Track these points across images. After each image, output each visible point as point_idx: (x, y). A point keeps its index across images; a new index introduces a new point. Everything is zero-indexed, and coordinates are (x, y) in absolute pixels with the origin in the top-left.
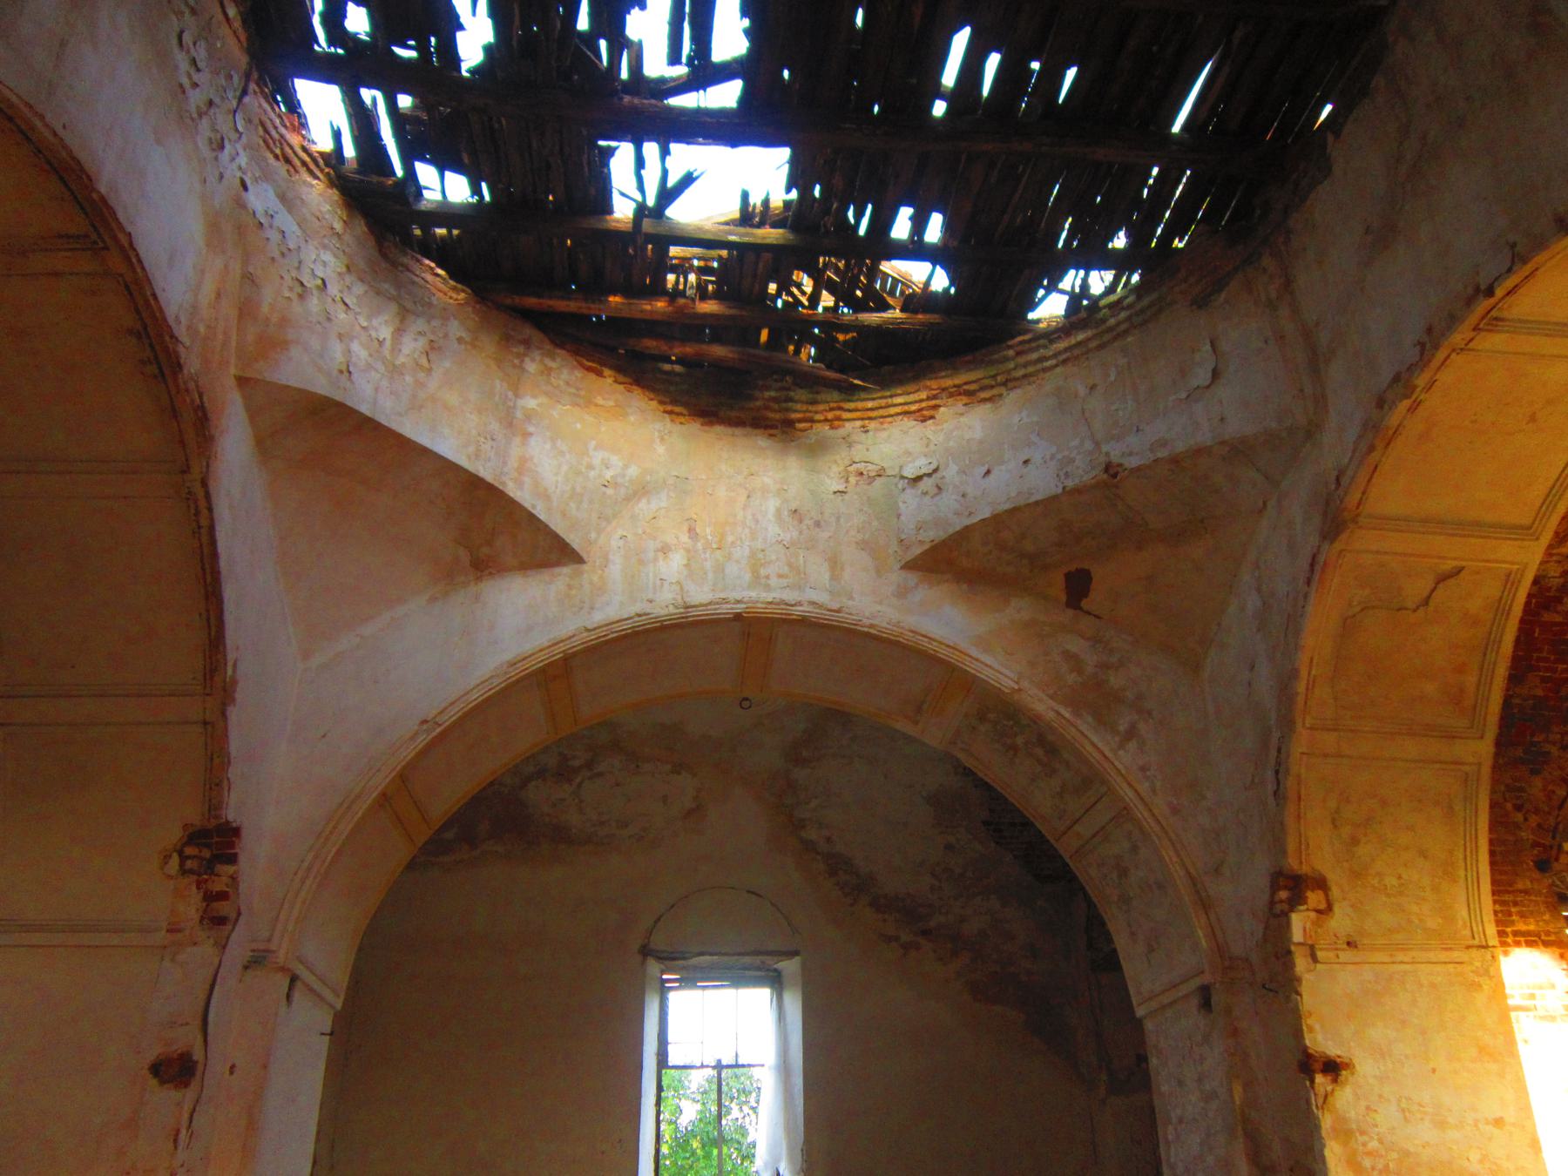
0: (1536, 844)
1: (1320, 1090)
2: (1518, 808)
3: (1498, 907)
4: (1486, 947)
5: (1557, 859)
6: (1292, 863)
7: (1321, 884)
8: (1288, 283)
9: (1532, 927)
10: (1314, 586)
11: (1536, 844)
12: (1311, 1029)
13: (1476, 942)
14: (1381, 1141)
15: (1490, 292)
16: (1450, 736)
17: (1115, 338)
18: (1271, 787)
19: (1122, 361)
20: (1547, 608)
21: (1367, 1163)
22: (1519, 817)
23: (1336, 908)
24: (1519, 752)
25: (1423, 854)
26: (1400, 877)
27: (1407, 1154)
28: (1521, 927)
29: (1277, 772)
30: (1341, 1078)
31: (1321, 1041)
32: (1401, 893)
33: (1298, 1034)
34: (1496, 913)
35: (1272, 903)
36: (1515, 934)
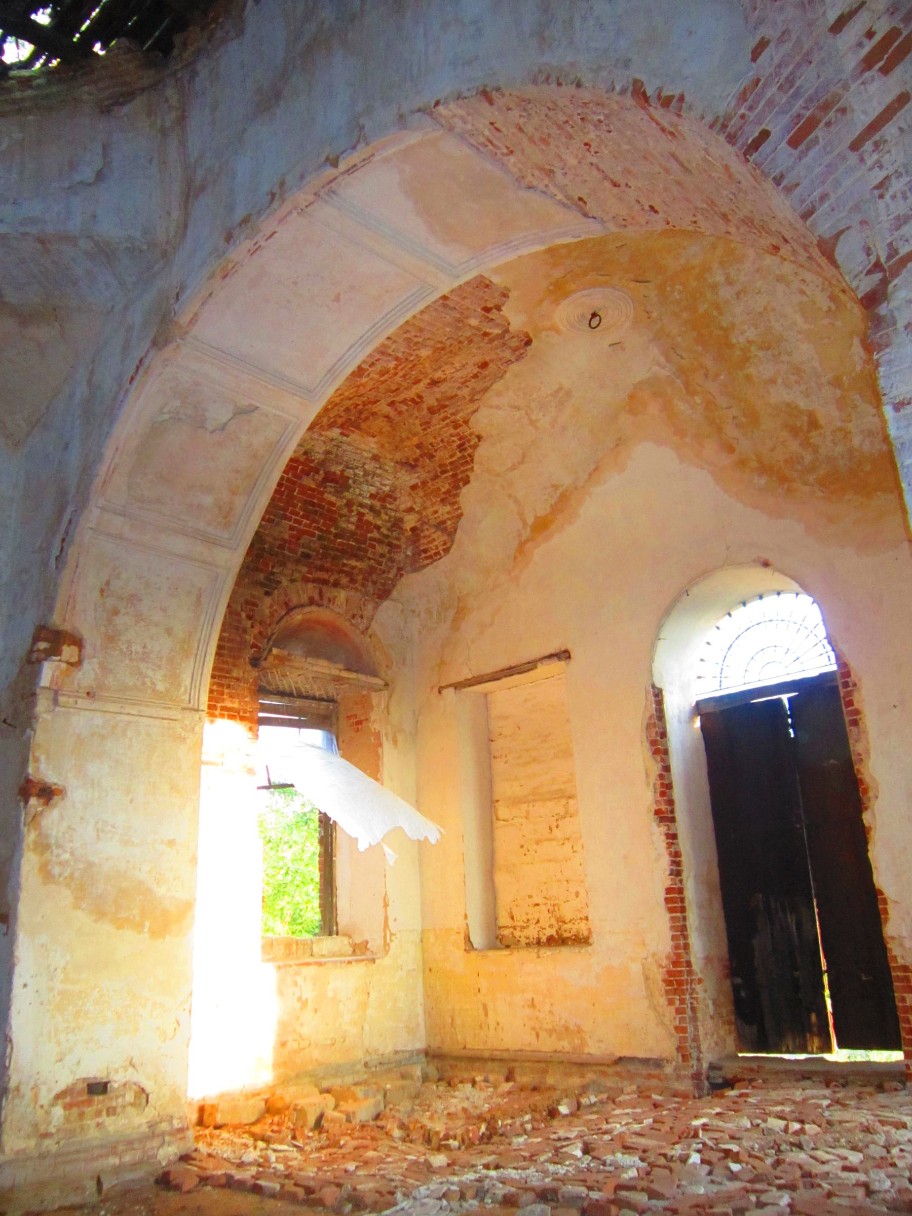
0: (254, 646)
1: (32, 811)
2: (250, 617)
3: (215, 688)
4: (197, 710)
5: (265, 659)
6: (56, 620)
7: (78, 643)
8: (182, 119)
9: (236, 705)
10: (135, 383)
11: (254, 646)
12: (37, 760)
13: (191, 706)
14: (72, 854)
15: (335, 164)
16: (214, 543)
17: (19, 111)
18: (55, 552)
19: (17, 135)
20: (308, 474)
21: (56, 870)
22: (249, 623)
23: (86, 665)
24: (261, 577)
25: (169, 631)
26: (145, 647)
27: (91, 865)
28: (229, 704)
29: (63, 540)
30: (52, 802)
31: (44, 770)
32: (143, 660)
33: (25, 762)
34: (211, 691)
35: (31, 651)
36: (223, 708)
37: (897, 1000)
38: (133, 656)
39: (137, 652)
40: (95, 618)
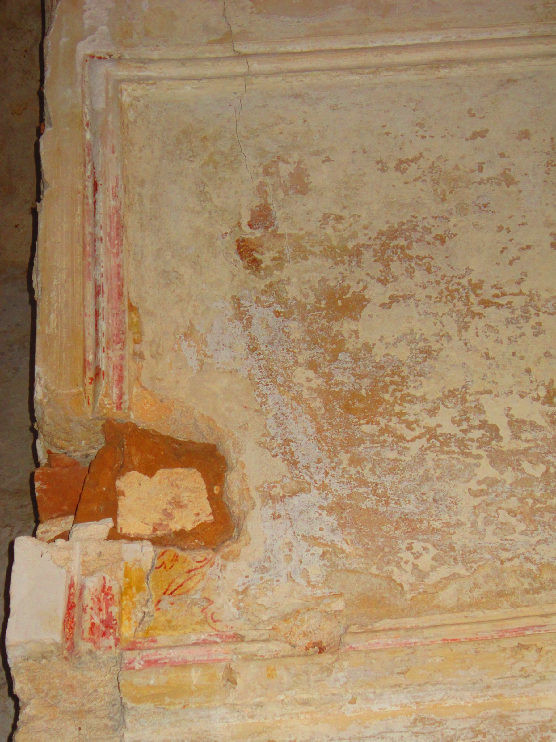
23: (259, 526)
37: (36, 490)
38: (507, 443)
39: (517, 426)
40: (253, 349)
